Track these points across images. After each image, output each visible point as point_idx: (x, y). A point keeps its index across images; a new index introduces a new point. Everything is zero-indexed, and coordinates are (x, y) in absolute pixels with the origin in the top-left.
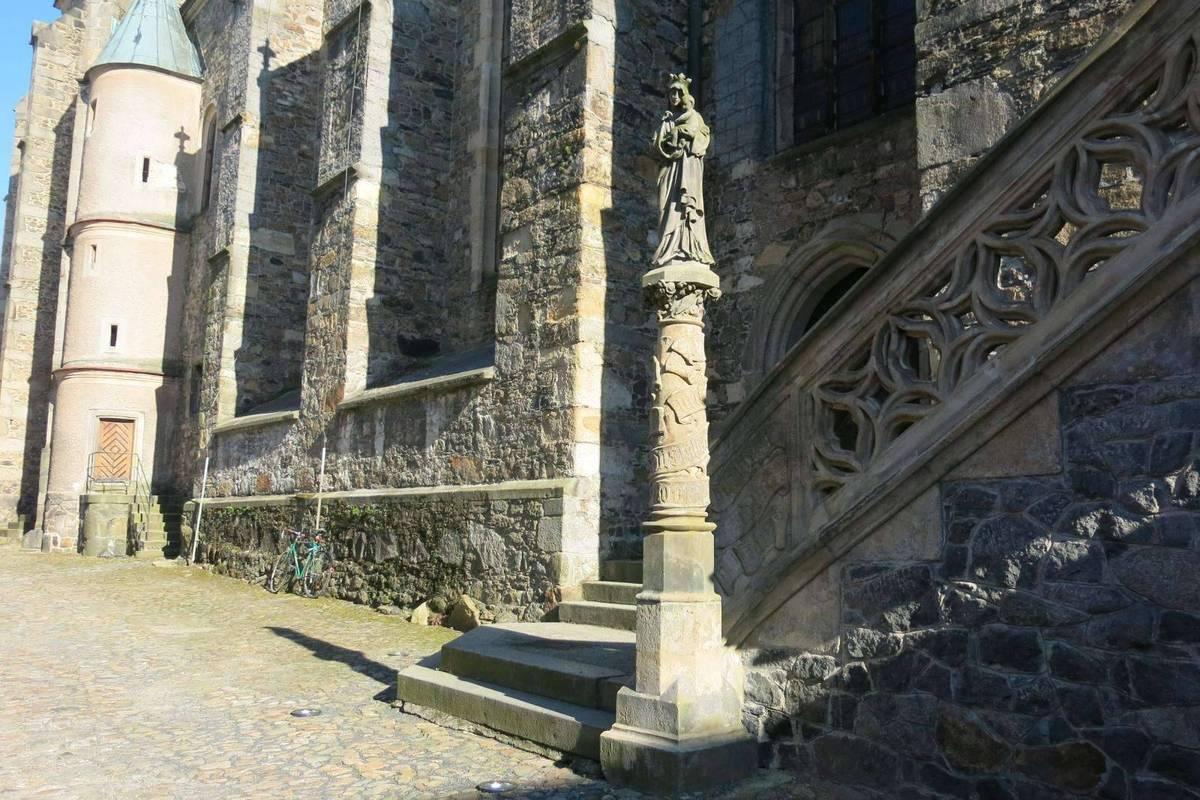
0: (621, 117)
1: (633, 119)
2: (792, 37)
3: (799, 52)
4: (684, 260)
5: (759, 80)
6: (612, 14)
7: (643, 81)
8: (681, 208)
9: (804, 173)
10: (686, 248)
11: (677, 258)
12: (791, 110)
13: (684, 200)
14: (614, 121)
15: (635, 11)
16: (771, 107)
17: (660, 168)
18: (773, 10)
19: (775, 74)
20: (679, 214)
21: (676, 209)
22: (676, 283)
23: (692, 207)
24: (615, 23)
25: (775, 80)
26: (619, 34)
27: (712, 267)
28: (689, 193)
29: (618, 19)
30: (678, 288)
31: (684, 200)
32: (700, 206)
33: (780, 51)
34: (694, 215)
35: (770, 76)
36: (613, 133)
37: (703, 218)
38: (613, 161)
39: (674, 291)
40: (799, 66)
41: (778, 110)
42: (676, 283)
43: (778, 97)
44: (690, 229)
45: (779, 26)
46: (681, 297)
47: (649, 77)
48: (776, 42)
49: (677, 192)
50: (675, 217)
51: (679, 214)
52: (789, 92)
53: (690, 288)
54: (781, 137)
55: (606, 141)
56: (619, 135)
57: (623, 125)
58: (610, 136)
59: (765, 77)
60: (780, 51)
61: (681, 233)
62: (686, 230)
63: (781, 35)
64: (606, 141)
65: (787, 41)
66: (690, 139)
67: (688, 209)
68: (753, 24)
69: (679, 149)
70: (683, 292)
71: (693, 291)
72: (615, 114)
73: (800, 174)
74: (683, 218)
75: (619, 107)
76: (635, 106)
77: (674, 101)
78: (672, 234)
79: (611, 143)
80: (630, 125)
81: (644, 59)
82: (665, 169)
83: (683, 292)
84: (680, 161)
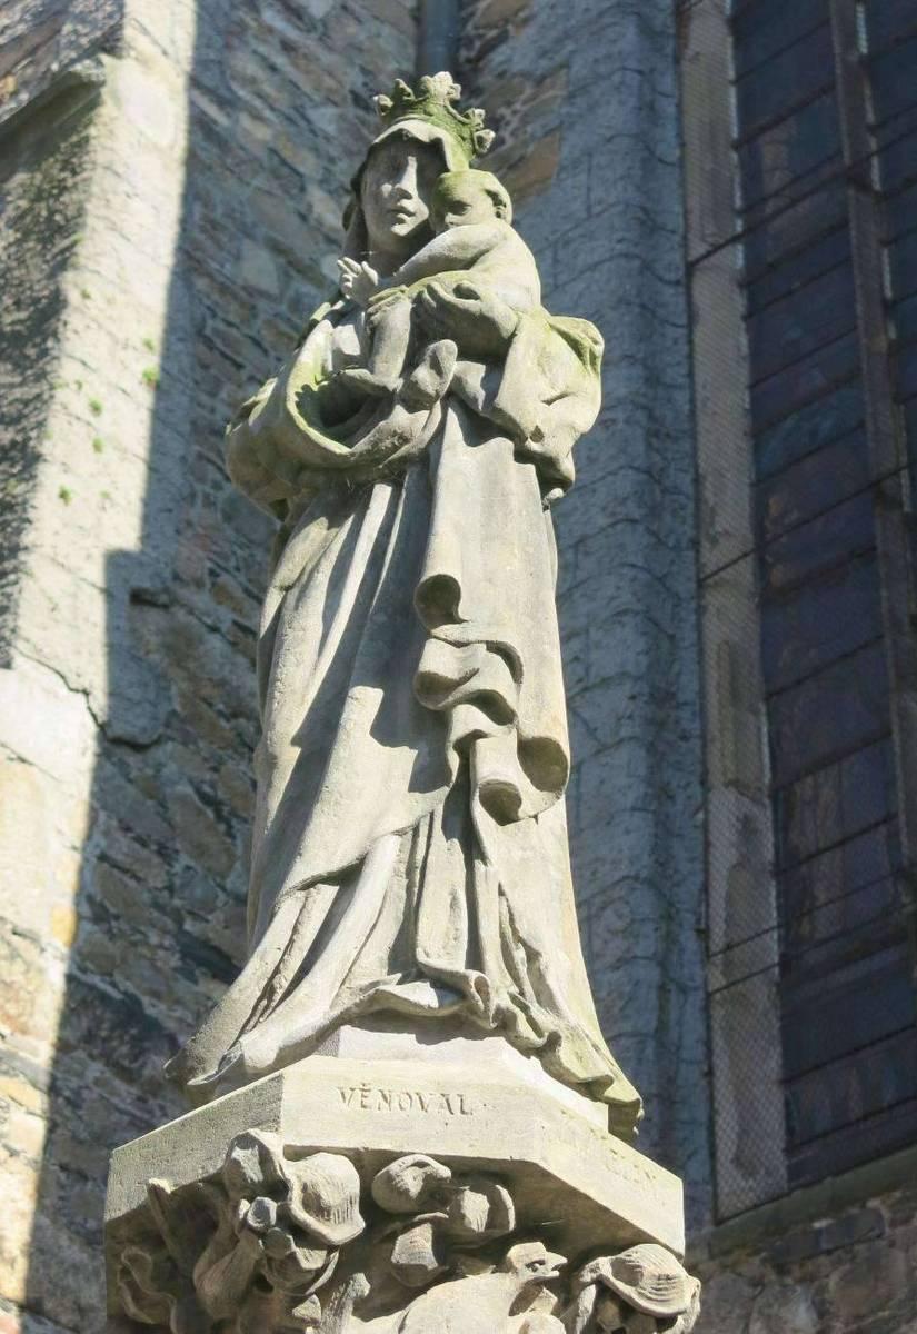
0: (89, 1038)
1: (138, 1053)
2: (764, 818)
3: (789, 867)
4: (432, 1028)
5: (647, 945)
6: (94, 671)
7: (188, 926)
8: (419, 715)
9: (848, 1280)
10: (440, 946)
11: (379, 1014)
12: (773, 1064)
13: (438, 658)
14: (63, 1047)
15: (179, 686)
16: (692, 1049)
17: (303, 518)
18: (694, 727)
19: (703, 933)
20: (404, 758)
21: (386, 730)
22: (371, 1164)
23: (490, 704)
24: (100, 700)
25: (707, 955)
26: (114, 743)
27: (620, 1121)
28: (479, 613)
29: (114, 693)
30: (384, 1213)
31: (438, 658)
32: (545, 709)
33: (724, 855)
34: (498, 762)
35: (690, 941)
36: (53, 1090)
37: (561, 806)
38: (41, 1192)
39: (346, 1228)
40: (794, 909)
41: (722, 1063)
42: (371, 1164)
43: (718, 1013)
44: (473, 849)
45: (716, 778)
46: (400, 1289)
47: (216, 918)
48: (705, 827)
49: (411, 602)
50: (372, 790)
51: (404, 758)
52: (762, 994)
53: (475, 1208)
54: (737, 1161)
55: (17, 1115)
56: (74, 1103)
57: (95, 1069)
58: (38, 1101)
59: (670, 939)
60: (724, 855)
61: (415, 876)
62: (446, 855)
63: (725, 808)
64: (17, 1115)
65: (747, 827)
66: (489, 346)
67: (467, 718)
68: (622, 756)
69: (415, 400)
70: (417, 1244)
71: (490, 1251)
72: (68, 1016)
73: (833, 1281)
74: (424, 780)
75: (81, 997)
76: (153, 1009)
77: (394, 214)
78: (347, 878)
79: (38, 1127)
80: (129, 1076)
81: (200, 851)
82: (316, 531)
83: (417, 1244)
84: (417, 475)
